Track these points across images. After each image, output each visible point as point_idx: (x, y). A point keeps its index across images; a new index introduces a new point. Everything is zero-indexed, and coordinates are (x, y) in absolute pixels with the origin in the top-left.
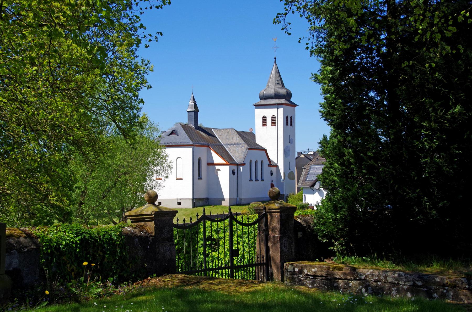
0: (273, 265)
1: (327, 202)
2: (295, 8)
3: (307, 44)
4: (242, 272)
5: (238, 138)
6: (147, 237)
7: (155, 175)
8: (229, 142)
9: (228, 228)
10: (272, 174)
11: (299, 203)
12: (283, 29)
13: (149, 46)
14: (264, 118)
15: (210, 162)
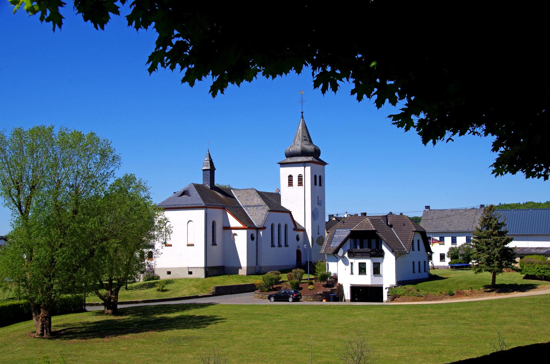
14: (290, 177)
15: (226, 225)
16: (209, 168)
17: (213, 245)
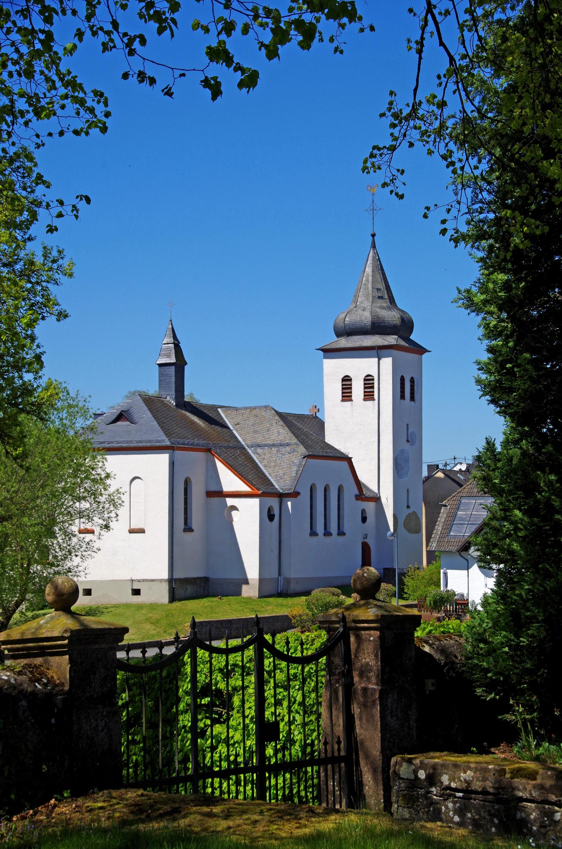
0: (362, 763)
1: (497, 603)
2: (415, 135)
3: (444, 222)
4: (288, 776)
5: (281, 430)
6: (49, 697)
7: (77, 521)
8: (259, 439)
9: (251, 665)
10: (364, 519)
11: (432, 590)
12: (385, 185)
13: (56, 229)
14: (347, 381)
15: (213, 488)
16: (173, 360)
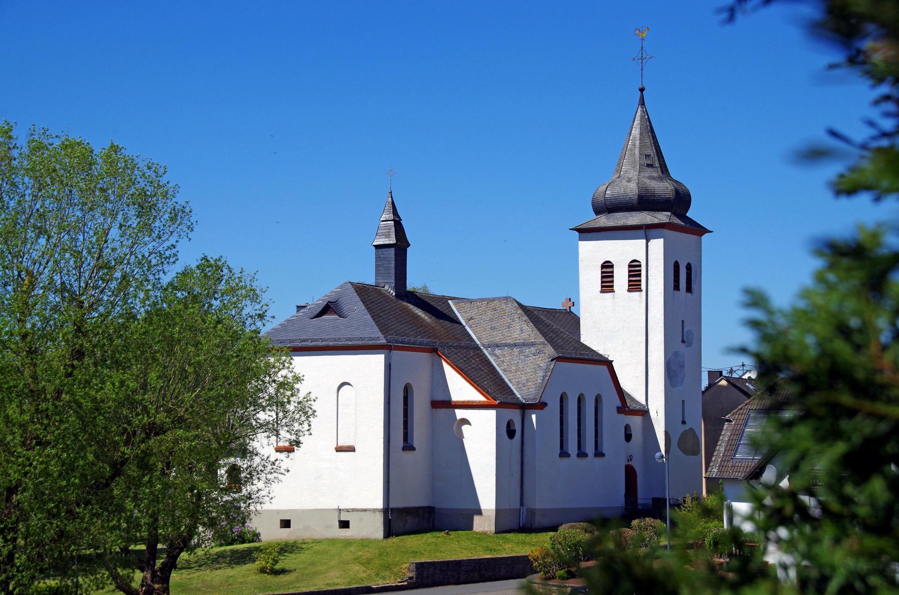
14: (607, 268)
15: (440, 397)
16: (393, 241)
17: (404, 449)
